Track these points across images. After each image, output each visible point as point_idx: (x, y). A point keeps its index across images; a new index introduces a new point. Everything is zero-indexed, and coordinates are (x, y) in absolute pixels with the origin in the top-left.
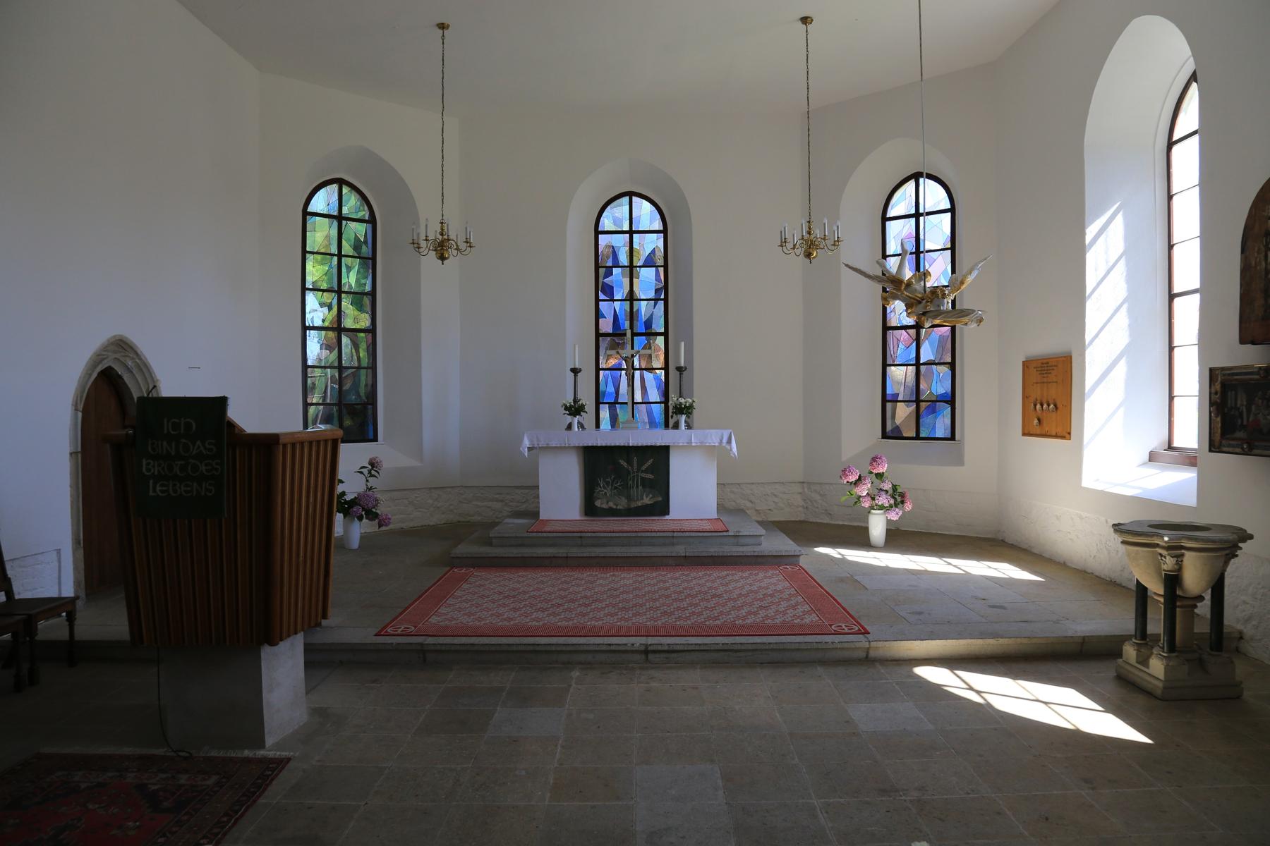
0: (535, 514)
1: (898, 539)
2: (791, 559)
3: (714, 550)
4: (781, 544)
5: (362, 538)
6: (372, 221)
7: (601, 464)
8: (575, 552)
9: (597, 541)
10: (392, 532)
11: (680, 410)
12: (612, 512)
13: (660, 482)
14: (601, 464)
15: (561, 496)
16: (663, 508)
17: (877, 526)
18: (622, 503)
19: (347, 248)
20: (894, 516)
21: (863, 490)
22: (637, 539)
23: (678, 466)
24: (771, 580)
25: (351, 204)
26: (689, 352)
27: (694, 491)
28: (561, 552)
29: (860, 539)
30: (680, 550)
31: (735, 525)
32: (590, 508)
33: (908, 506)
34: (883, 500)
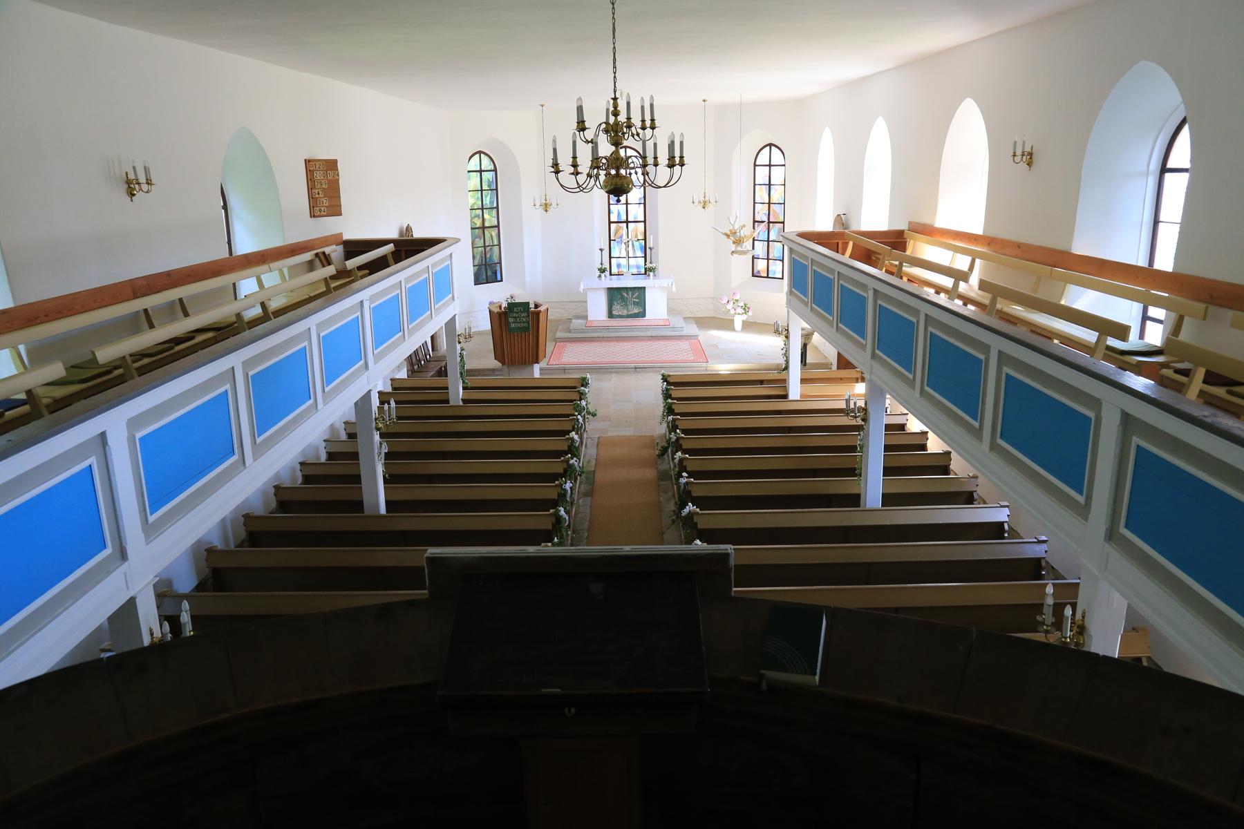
0: (586, 317)
1: (748, 326)
2: (695, 337)
3: (664, 333)
4: (692, 329)
5: (419, 397)
6: (495, 170)
7: (615, 294)
8: (606, 335)
9: (616, 329)
10: (978, 469)
11: (651, 270)
12: (621, 316)
13: (641, 303)
14: (615, 294)
15: (597, 309)
16: (643, 314)
17: (738, 322)
18: (625, 313)
19: (485, 187)
20: (744, 317)
21: (730, 306)
22: (632, 328)
23: (649, 295)
24: (685, 345)
25: (486, 164)
26: (656, 240)
27: (656, 307)
28: (601, 335)
29: (728, 325)
30: (649, 333)
31: (678, 322)
32: (611, 315)
33: (750, 314)
34: (740, 310)
